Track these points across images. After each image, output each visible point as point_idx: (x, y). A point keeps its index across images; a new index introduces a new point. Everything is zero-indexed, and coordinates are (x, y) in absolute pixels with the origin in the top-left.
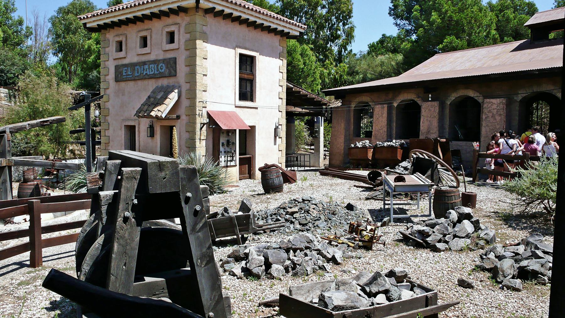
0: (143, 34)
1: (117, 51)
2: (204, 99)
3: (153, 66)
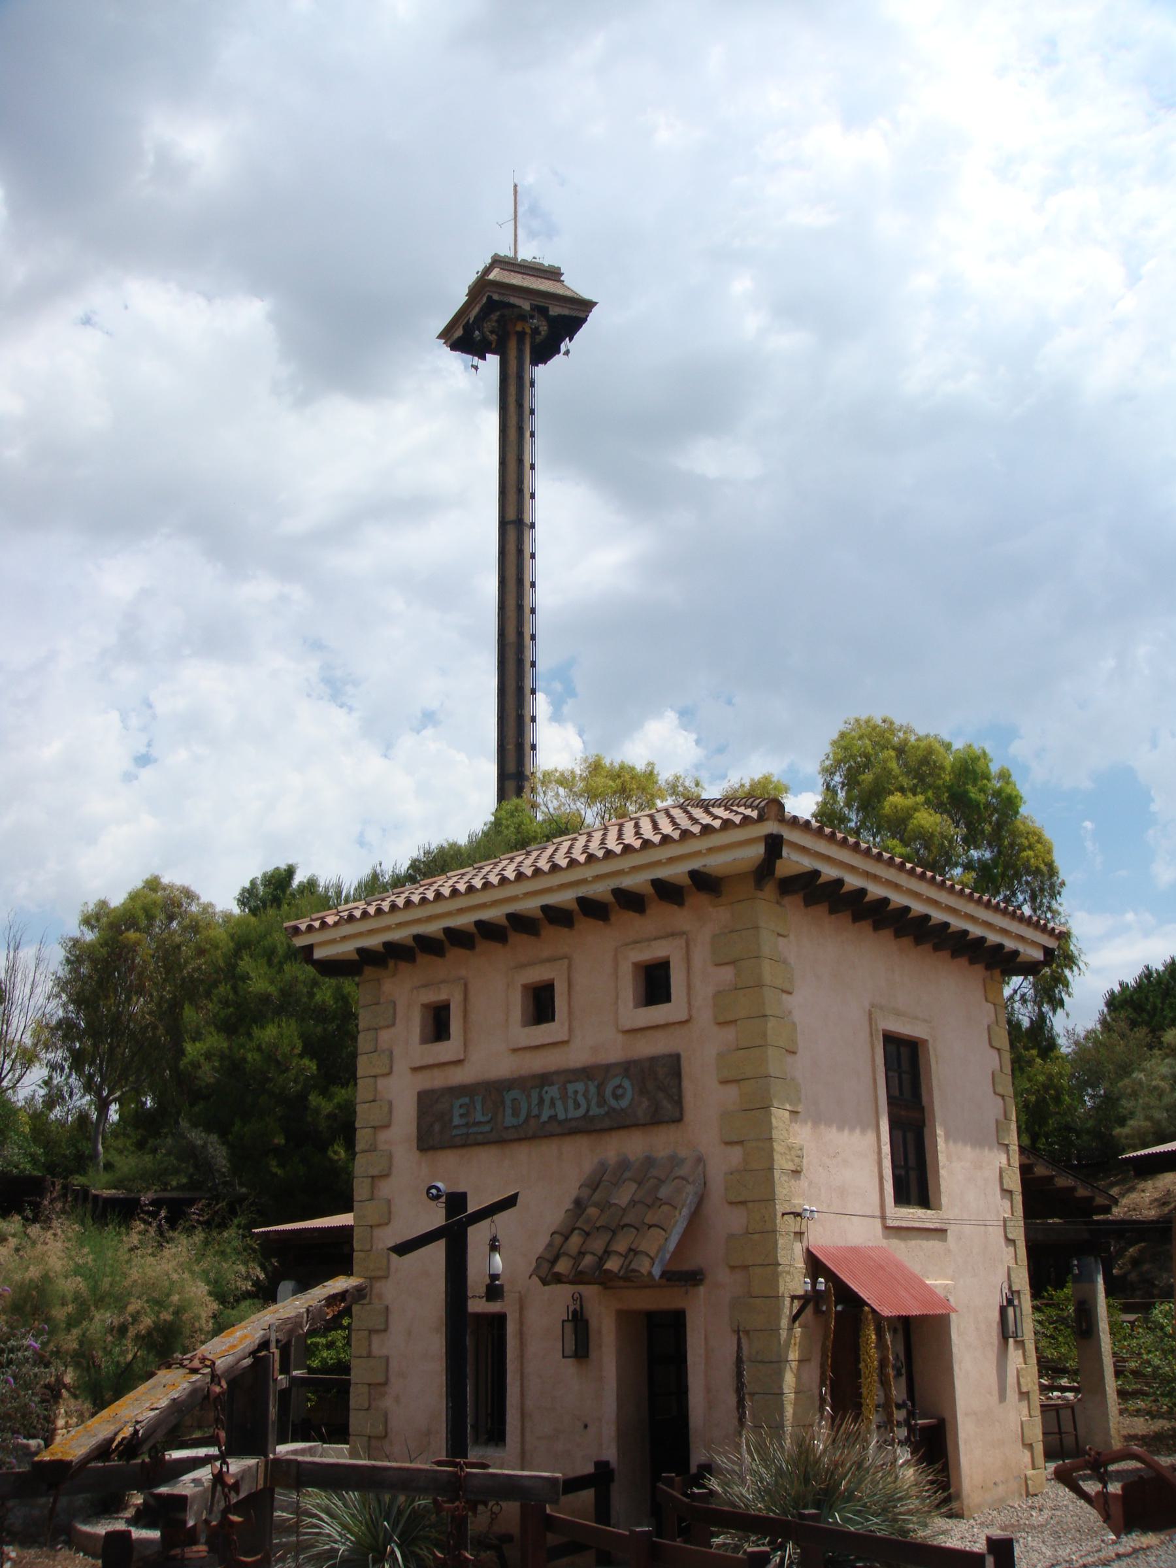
0: (537, 975)
1: (424, 1040)
2: (800, 1203)
3: (580, 1087)
